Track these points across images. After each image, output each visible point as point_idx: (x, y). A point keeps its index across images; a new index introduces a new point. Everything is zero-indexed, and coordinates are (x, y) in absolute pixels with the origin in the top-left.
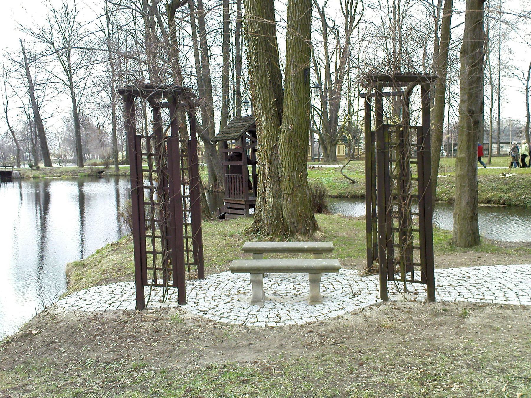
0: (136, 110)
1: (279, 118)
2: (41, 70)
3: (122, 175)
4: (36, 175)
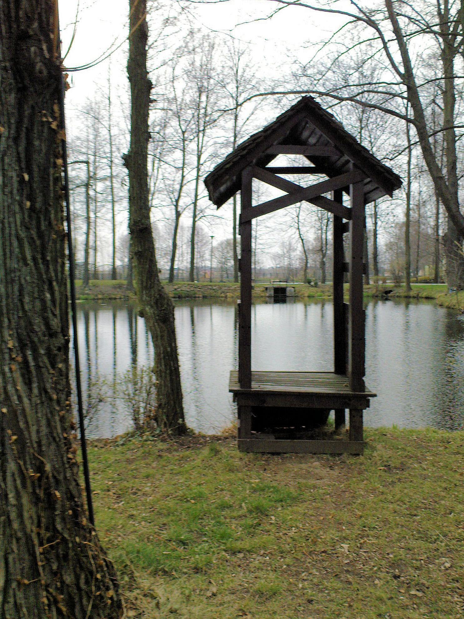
0: (198, 248)
1: (30, 389)
2: (101, 87)
3: (414, 297)
4: (312, 293)
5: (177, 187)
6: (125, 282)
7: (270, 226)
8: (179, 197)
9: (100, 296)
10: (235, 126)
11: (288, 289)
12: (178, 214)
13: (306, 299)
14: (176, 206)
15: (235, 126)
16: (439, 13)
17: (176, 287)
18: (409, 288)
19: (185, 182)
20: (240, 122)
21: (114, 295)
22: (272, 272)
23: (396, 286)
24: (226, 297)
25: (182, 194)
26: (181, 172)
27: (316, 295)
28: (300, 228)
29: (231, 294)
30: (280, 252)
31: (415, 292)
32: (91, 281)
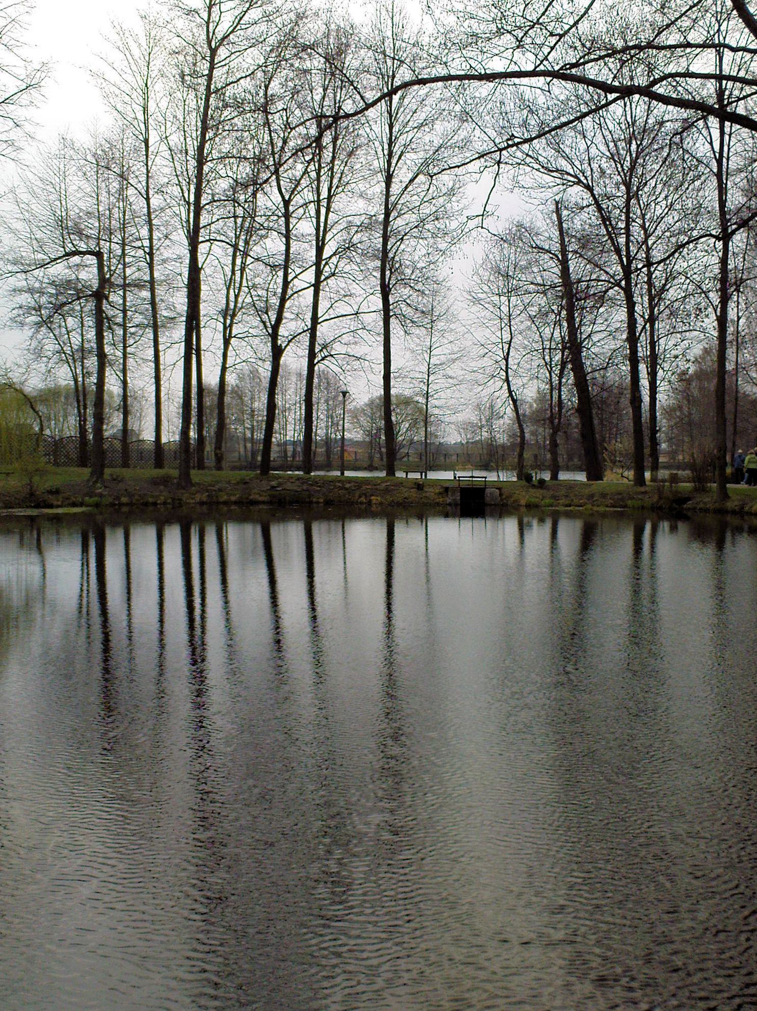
5: (275, 301)
6: (175, 473)
7: (453, 375)
8: (279, 319)
9: (124, 500)
10: (388, 195)
11: (488, 491)
12: (277, 352)
13: (523, 509)
14: (274, 336)
15: (388, 195)
16: (561, 336)
17: (274, 483)
18: (724, 494)
19: (290, 292)
20: (396, 188)
21: (152, 497)
22: (459, 451)
23: (696, 490)
24: (369, 503)
25: (286, 314)
26: (281, 273)
27: (543, 503)
28: (510, 379)
29: (379, 498)
30: (474, 419)
31: (736, 503)
32: (107, 471)
